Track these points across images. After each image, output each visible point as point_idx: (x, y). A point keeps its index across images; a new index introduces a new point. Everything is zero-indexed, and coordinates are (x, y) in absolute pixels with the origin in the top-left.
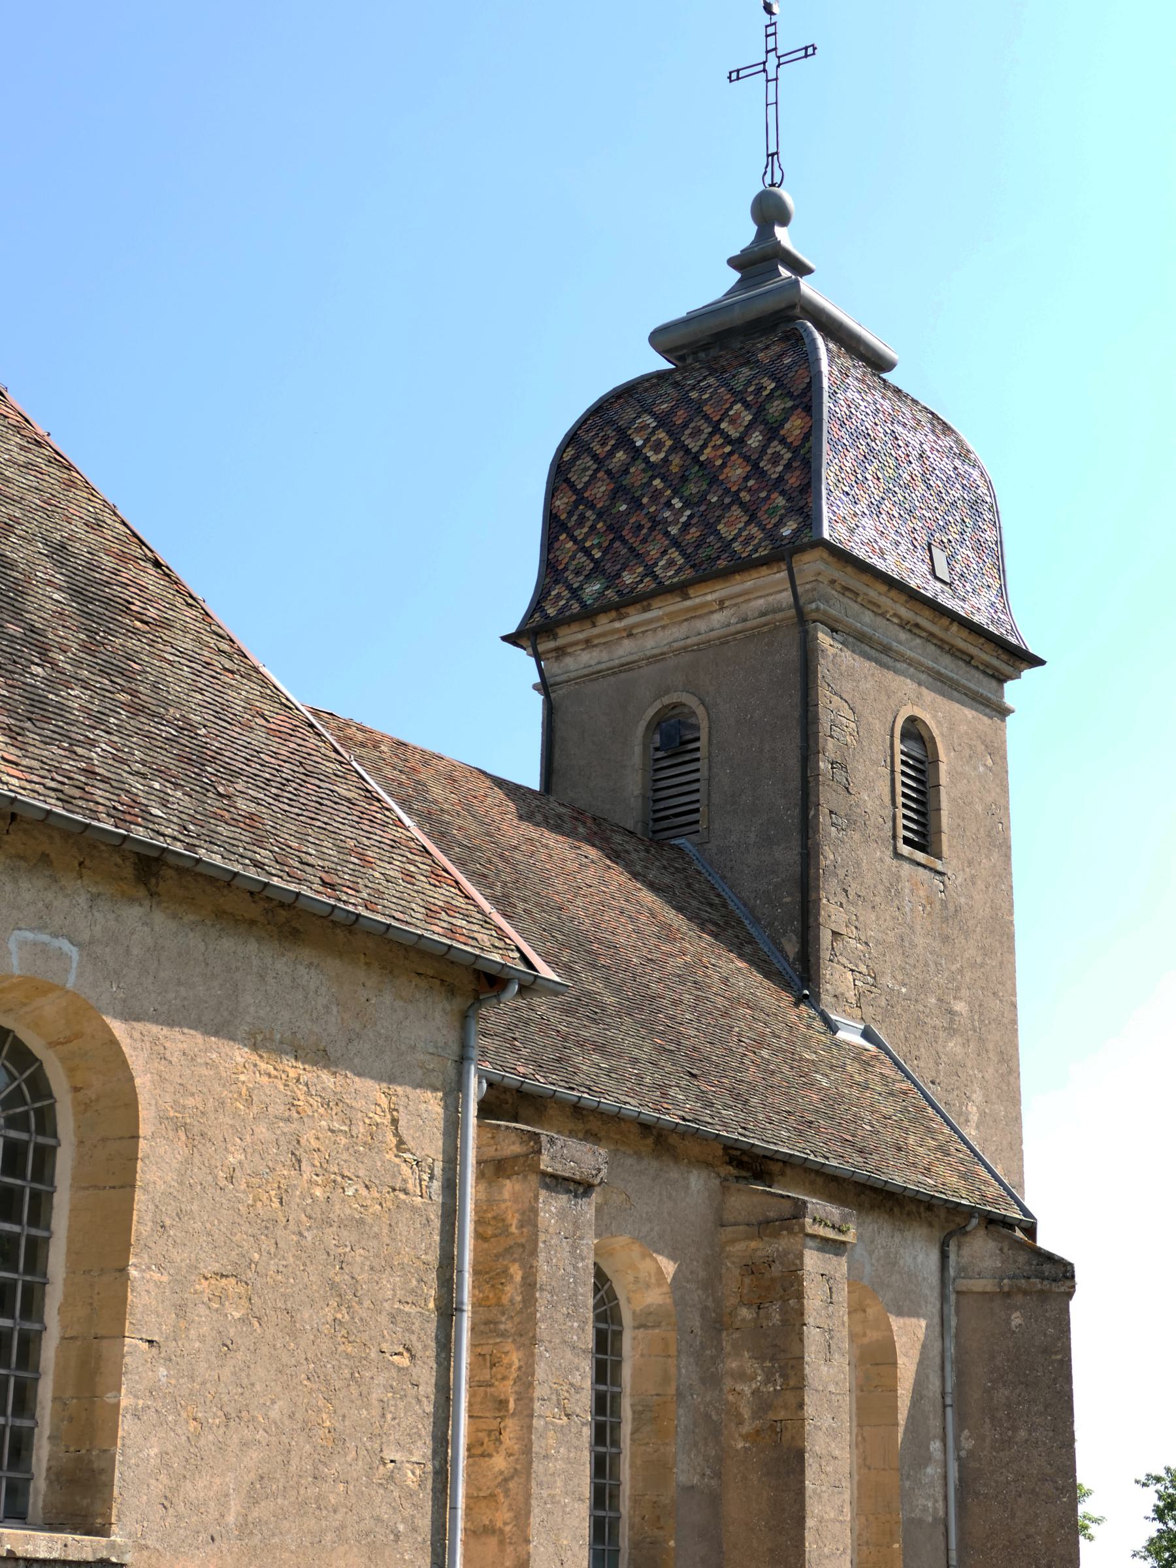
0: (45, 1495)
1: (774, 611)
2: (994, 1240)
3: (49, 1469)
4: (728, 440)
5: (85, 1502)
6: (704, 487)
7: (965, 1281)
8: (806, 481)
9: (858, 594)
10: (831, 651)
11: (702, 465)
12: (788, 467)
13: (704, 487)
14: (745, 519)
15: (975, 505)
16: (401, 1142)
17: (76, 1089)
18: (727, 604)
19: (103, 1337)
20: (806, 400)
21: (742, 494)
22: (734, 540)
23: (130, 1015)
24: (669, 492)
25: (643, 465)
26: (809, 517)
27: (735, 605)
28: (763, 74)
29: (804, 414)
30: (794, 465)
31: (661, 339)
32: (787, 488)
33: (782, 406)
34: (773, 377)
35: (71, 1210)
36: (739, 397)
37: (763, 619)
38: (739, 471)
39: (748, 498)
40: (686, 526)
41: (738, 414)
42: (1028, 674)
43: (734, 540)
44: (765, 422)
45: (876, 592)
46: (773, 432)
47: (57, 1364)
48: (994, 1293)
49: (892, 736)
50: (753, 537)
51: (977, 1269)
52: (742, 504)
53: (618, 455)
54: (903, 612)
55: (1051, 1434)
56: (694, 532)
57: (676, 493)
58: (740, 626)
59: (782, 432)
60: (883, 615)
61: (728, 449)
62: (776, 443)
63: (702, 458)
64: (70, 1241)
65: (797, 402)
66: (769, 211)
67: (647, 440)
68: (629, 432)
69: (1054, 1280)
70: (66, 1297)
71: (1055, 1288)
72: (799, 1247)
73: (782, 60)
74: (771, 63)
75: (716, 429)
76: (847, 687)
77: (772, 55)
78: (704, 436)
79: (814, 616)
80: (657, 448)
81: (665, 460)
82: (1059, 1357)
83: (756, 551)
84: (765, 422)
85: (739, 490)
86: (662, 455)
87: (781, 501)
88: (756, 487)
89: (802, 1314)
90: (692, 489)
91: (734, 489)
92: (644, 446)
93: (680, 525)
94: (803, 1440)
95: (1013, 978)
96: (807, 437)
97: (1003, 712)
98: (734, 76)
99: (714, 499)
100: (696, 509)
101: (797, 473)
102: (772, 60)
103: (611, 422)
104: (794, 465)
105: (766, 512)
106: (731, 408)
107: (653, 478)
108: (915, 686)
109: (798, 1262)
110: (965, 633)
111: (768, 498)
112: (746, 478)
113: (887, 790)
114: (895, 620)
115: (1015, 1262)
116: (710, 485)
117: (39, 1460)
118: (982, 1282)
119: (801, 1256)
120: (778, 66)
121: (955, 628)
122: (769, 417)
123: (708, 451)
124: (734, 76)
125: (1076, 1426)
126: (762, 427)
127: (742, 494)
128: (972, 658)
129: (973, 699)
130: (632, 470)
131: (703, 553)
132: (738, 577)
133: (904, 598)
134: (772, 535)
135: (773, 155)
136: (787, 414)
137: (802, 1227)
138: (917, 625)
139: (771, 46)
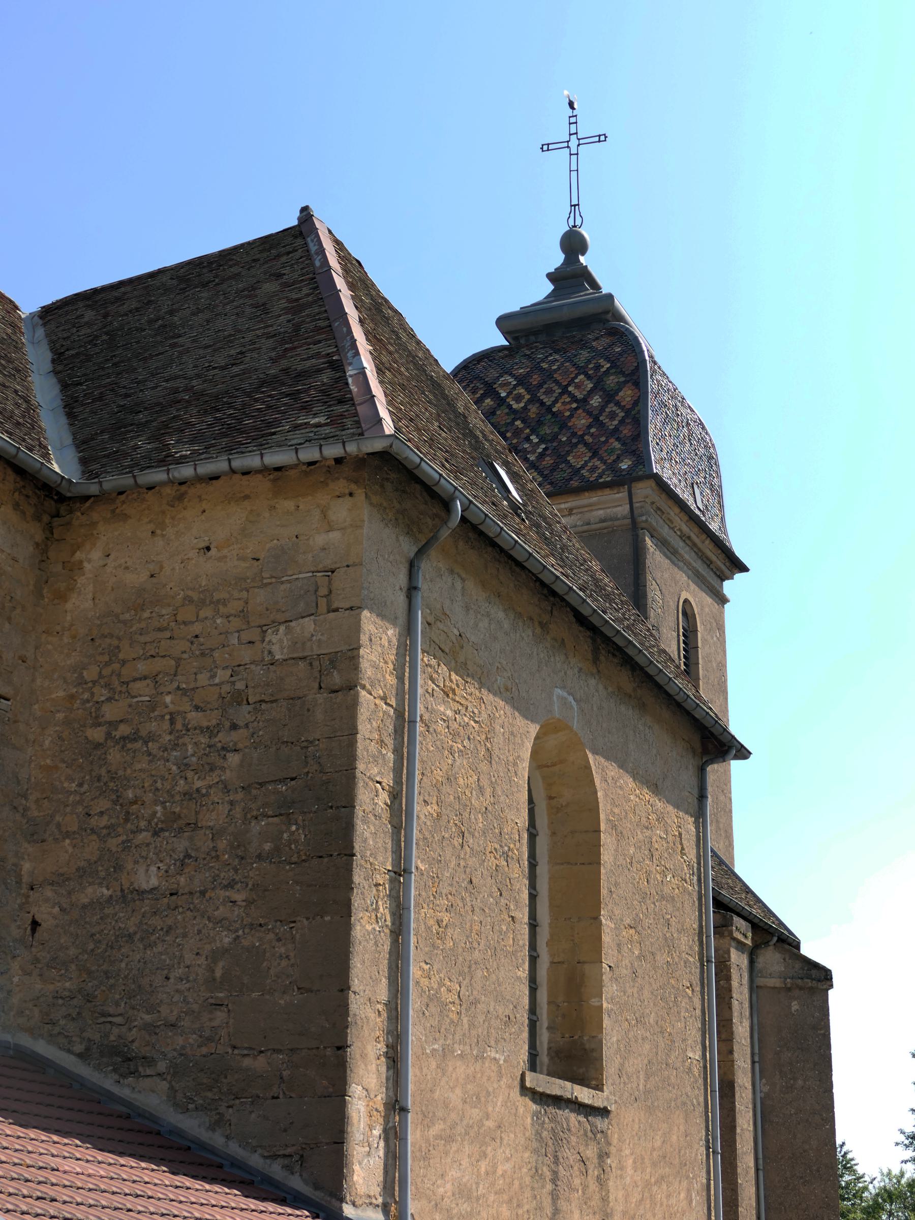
0: (548, 1066)
1: (611, 519)
2: (780, 953)
3: (549, 1049)
4: (574, 399)
5: (581, 1071)
6: (556, 430)
7: (762, 979)
8: (636, 433)
9: (663, 513)
10: (652, 550)
11: (554, 414)
12: (622, 422)
13: (556, 430)
14: (589, 454)
15: (710, 458)
16: (683, 849)
17: (551, 798)
18: (574, 511)
19: (584, 963)
20: (635, 377)
21: (586, 437)
22: (583, 467)
23: (595, 752)
24: (528, 431)
25: (507, 410)
26: (642, 458)
27: (581, 513)
28: (567, 150)
29: (633, 387)
30: (627, 421)
31: (503, 322)
32: (621, 436)
33: (616, 380)
34: (608, 359)
35: (550, 878)
36: (582, 371)
37: (604, 524)
38: (583, 421)
39: (591, 440)
40: (542, 456)
41: (582, 382)
42: (739, 576)
43: (583, 467)
44: (603, 389)
45: (674, 512)
46: (610, 397)
47: (549, 980)
48: (781, 988)
49: (678, 612)
50: (597, 467)
51: (769, 972)
52: (586, 444)
53: (486, 401)
54: (685, 528)
55: (818, 1083)
56: (548, 461)
57: (533, 431)
58: (586, 528)
59: (617, 398)
60: (673, 529)
61: (574, 405)
62: (612, 405)
63: (554, 410)
64: (551, 899)
65: (628, 379)
66: (573, 244)
67: (509, 393)
68: (495, 386)
69: (819, 981)
70: (552, 935)
71: (820, 985)
72: (727, 946)
73: (581, 141)
74: (574, 142)
75: (565, 391)
76: (658, 575)
77: (574, 137)
78: (555, 395)
79: (643, 525)
80: (518, 398)
81: (525, 408)
82: (822, 1032)
83: (601, 477)
84: (603, 389)
85: (584, 435)
86: (522, 405)
87: (617, 445)
88: (597, 433)
89: (731, 991)
90: (546, 430)
91: (580, 433)
92: (507, 396)
93: (537, 455)
94: (734, 1075)
95: (730, 782)
96: (636, 403)
97: (722, 600)
98: (545, 148)
99: (564, 439)
100: (550, 445)
101: (629, 427)
102: (574, 142)
103: (478, 378)
104: (627, 421)
105: (606, 451)
106: (576, 377)
107: (514, 420)
108: (686, 579)
109: (726, 956)
110: (711, 546)
111: (606, 442)
112: (590, 426)
113: (676, 647)
114: (679, 533)
115: (793, 967)
116: (561, 429)
117: (541, 1043)
118: (773, 980)
119: (729, 952)
120: (579, 145)
121: (708, 541)
122: (606, 387)
123: (558, 405)
124: (545, 148)
125: (834, 1078)
126: (601, 393)
127: (586, 437)
128: (711, 562)
129: (711, 591)
130: (498, 413)
131: (558, 475)
132: (587, 494)
133: (686, 518)
134: (612, 467)
135: (575, 206)
136: (620, 387)
137: (731, 933)
138: (689, 538)
139: (573, 131)
